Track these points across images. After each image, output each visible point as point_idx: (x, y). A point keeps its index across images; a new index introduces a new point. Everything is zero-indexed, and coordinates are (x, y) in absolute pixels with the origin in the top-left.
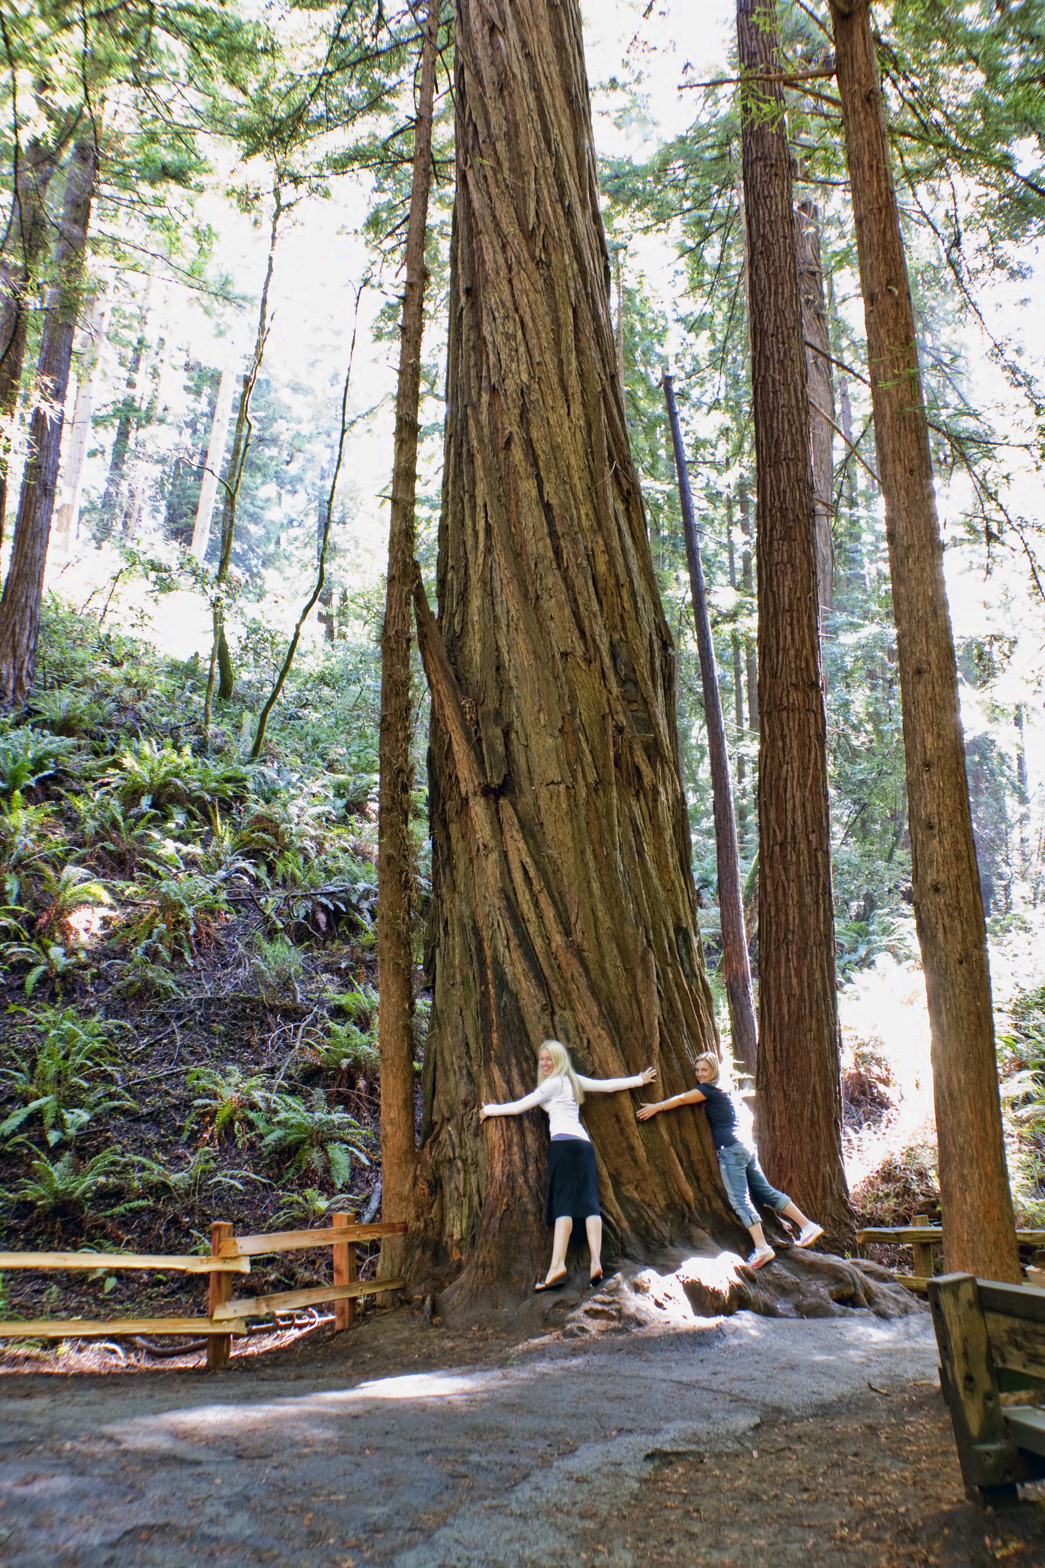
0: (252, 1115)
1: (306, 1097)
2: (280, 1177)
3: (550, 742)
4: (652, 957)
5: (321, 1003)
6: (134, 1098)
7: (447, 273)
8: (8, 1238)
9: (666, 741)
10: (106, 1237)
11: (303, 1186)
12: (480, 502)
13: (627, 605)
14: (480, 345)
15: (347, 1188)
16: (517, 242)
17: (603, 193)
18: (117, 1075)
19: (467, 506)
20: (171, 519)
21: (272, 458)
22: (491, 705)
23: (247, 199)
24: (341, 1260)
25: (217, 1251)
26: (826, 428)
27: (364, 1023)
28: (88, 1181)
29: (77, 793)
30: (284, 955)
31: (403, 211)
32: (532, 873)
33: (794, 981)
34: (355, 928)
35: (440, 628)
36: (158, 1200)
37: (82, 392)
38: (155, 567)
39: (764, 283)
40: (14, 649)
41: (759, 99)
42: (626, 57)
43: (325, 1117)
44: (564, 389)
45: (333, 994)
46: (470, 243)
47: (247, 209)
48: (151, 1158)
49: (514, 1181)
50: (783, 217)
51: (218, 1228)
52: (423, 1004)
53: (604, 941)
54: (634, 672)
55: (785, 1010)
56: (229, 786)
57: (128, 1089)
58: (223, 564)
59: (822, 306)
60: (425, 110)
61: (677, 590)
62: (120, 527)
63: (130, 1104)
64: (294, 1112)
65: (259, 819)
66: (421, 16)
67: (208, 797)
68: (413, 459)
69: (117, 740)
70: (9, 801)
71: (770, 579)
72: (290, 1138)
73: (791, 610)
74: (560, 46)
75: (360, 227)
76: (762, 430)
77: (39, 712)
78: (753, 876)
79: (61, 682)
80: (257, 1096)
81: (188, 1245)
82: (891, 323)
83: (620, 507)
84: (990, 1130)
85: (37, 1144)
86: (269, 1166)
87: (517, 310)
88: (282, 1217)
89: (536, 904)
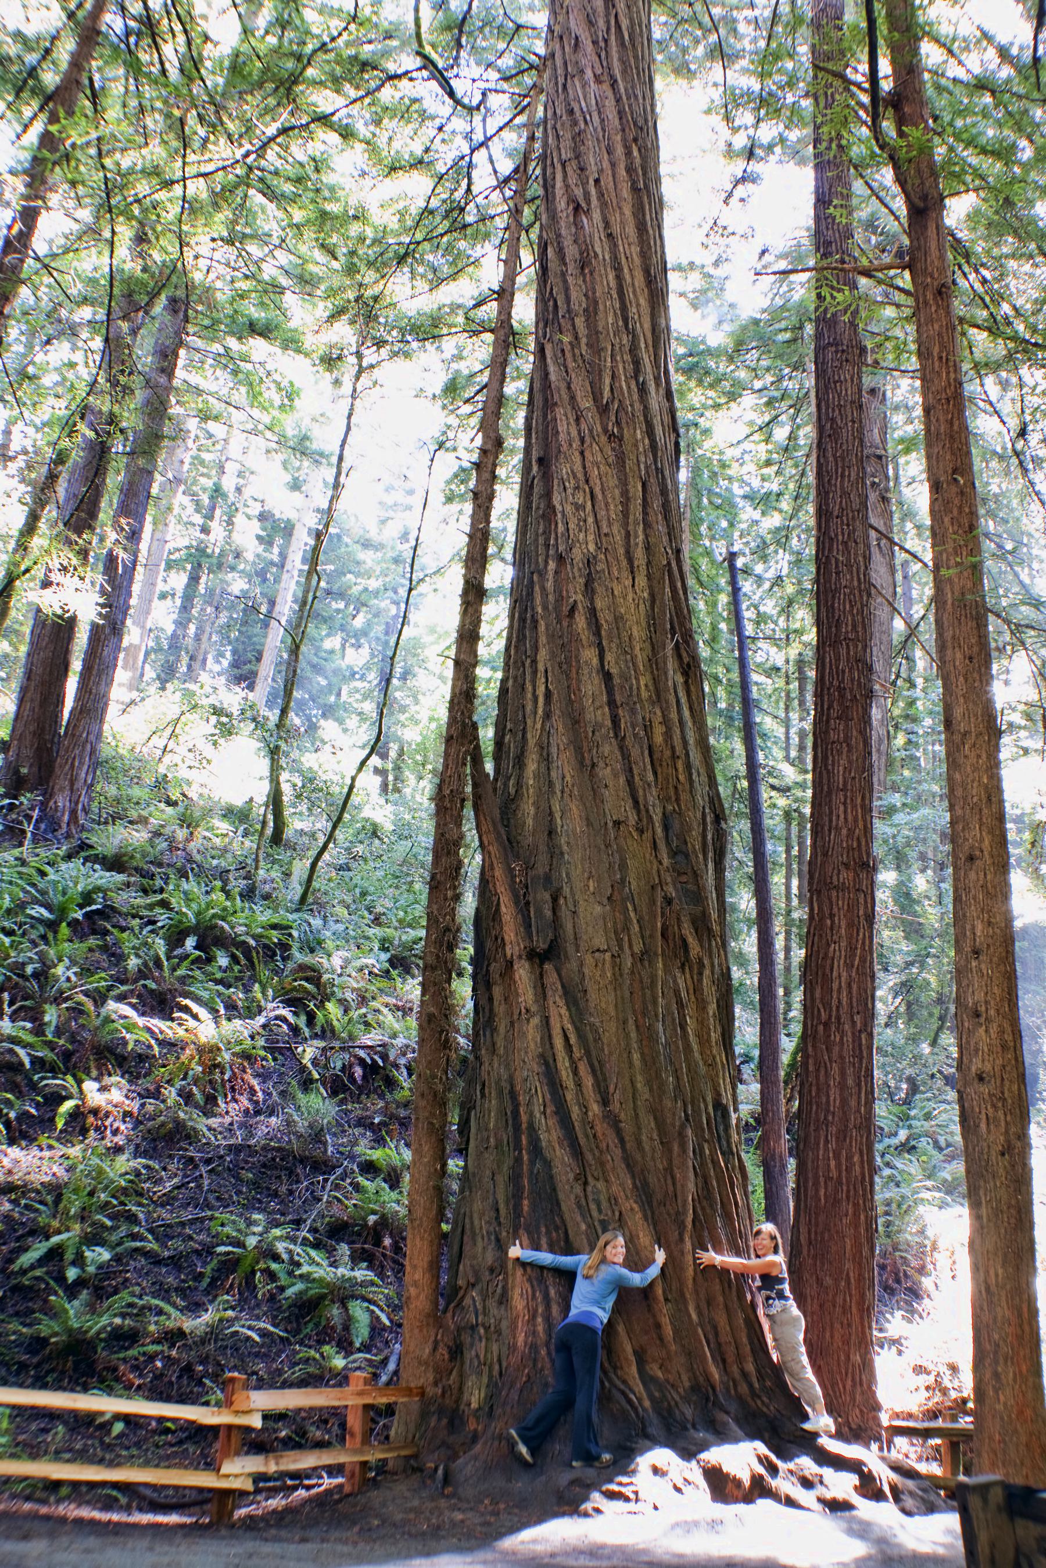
0: (274, 1266)
1: (330, 1252)
2: (298, 1331)
3: (598, 909)
4: (689, 1132)
5: (352, 1157)
6: (157, 1239)
7: (521, 443)
8: (18, 1373)
9: (714, 915)
10: (117, 1379)
11: (321, 1342)
12: (541, 667)
13: (682, 778)
14: (549, 514)
15: (366, 1348)
16: (591, 416)
17: (677, 371)
18: (141, 1216)
19: (528, 671)
20: (235, 664)
21: (338, 611)
22: (541, 870)
23: (330, 361)
24: (355, 1422)
25: (228, 1403)
26: (887, 609)
27: (393, 1180)
28: (104, 1321)
29: (123, 930)
30: (318, 1106)
31: (484, 378)
32: (573, 1040)
33: (833, 1163)
34: (391, 1083)
35: (495, 790)
36: (173, 1345)
37: (158, 535)
38: (217, 711)
39: (831, 466)
40: (72, 784)
41: (832, 288)
42: (705, 240)
43: (348, 1274)
44: (630, 560)
45: (366, 1150)
46: (545, 416)
47: (330, 369)
48: (169, 1302)
49: (537, 1352)
50: (853, 402)
51: (232, 1380)
52: (455, 1165)
53: (642, 1113)
54: (685, 834)
55: (822, 1192)
56: (274, 932)
57: (151, 1231)
58: (284, 712)
59: (887, 490)
60: (508, 283)
61: (730, 749)
62: (184, 669)
63: (153, 1246)
64: (319, 1267)
65: (302, 967)
66: (508, 193)
67: (253, 943)
68: (477, 622)
69: (166, 880)
70: (56, 932)
71: (825, 758)
72: (311, 1292)
73: (844, 789)
74: (641, 228)
75: (438, 392)
76: (823, 609)
77: (91, 847)
78: (795, 1054)
79: (115, 818)
80: (281, 1247)
81: (200, 1395)
82: (955, 512)
83: (680, 679)
84: (1027, 1328)
85: (55, 1280)
86: (288, 1319)
87: (587, 481)
88: (298, 1372)
89: (575, 1072)
